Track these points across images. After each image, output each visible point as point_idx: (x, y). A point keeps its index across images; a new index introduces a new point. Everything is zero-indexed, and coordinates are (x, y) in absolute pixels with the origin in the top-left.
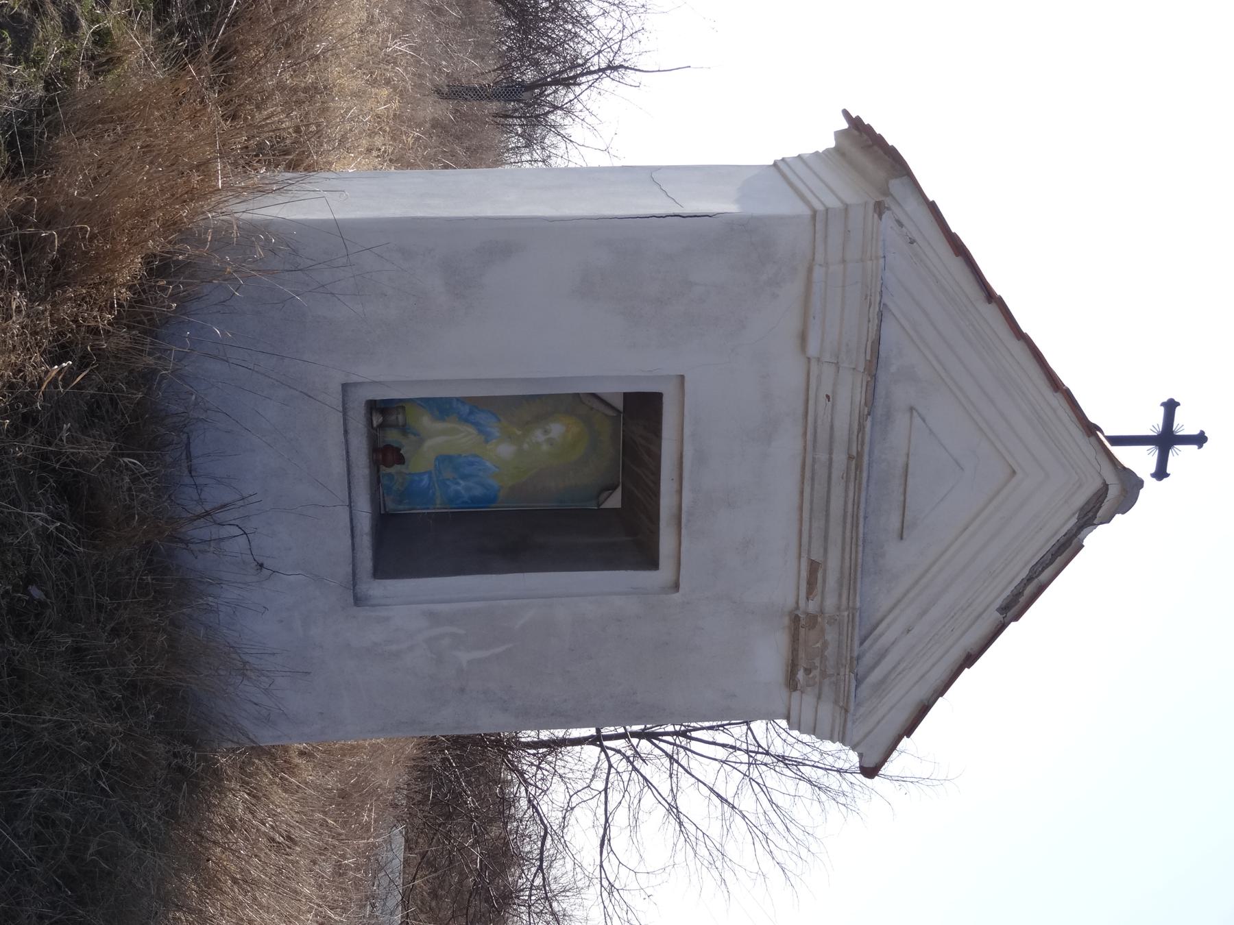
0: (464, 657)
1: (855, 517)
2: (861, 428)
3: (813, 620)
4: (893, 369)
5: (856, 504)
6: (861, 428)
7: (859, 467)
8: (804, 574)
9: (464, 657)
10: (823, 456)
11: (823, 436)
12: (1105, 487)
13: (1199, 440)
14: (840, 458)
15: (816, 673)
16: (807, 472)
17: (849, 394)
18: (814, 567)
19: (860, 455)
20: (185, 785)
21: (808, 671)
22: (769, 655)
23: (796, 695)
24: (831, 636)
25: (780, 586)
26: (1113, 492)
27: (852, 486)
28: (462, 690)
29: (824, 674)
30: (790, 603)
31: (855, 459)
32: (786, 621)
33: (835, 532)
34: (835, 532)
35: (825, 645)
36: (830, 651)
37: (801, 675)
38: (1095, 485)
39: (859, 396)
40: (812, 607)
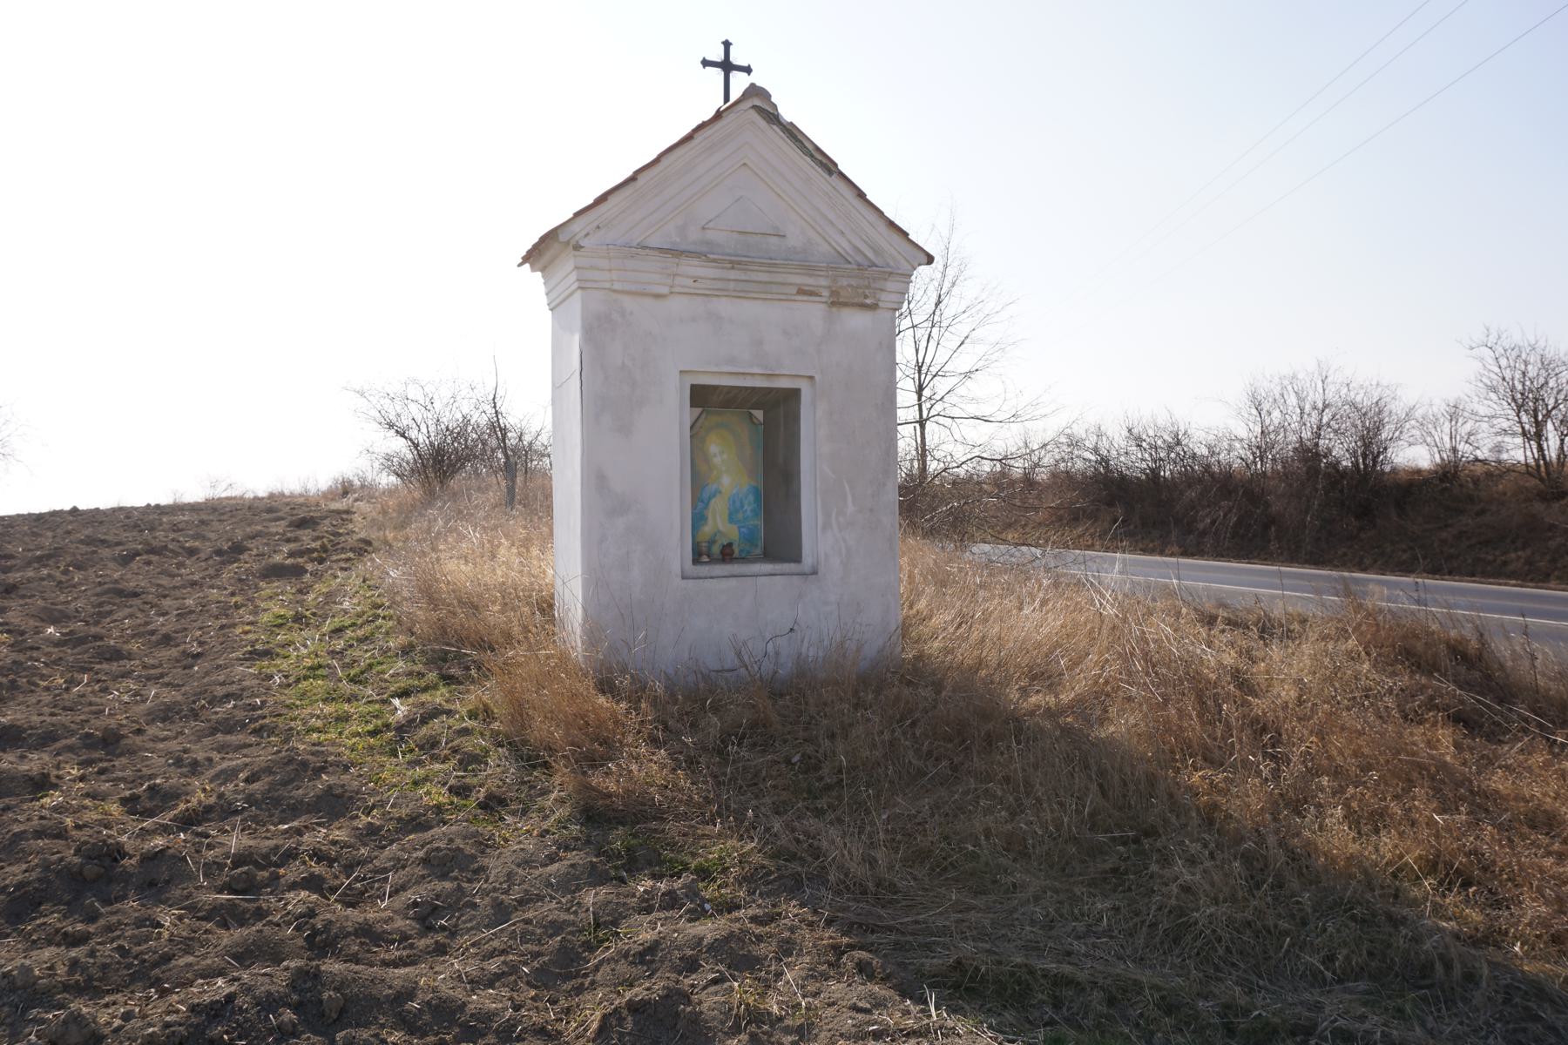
1: (770, 265)
2: (714, 261)
3: (834, 293)
5: (762, 264)
6: (714, 261)
7: (739, 263)
10: (732, 285)
11: (719, 285)
12: (754, 107)
14: (733, 274)
16: (740, 295)
17: (692, 268)
18: (801, 292)
19: (731, 262)
21: (866, 297)
22: (855, 320)
24: (844, 282)
25: (813, 313)
26: (757, 102)
28: (871, 510)
29: (868, 287)
31: (734, 265)
33: (779, 278)
34: (779, 278)
36: (854, 282)
37: (868, 301)
38: (753, 113)
39: (695, 262)
40: (826, 293)
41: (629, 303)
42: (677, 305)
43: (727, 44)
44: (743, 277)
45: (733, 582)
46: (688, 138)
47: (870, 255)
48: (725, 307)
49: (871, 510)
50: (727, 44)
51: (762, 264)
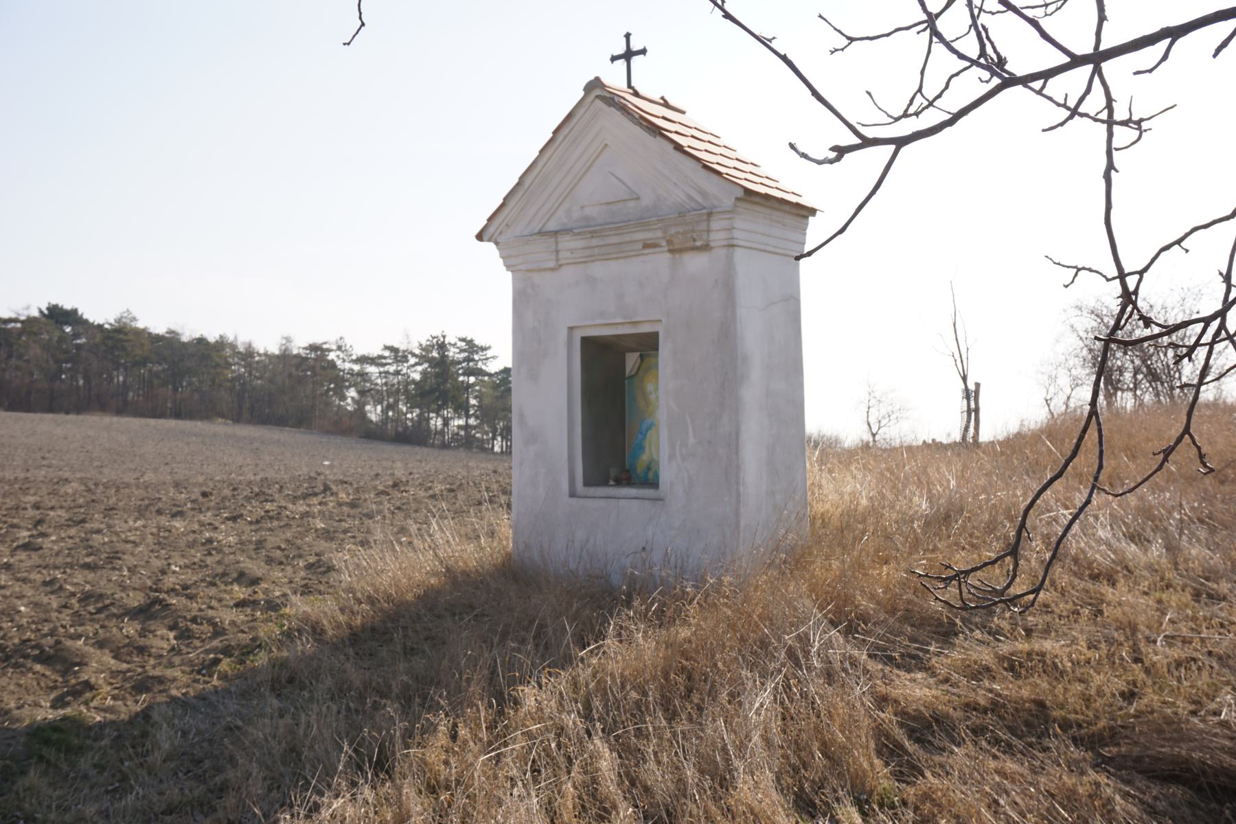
0: (692, 441)
1: (616, 229)
2: (579, 234)
3: (669, 242)
4: (566, 220)
5: (611, 229)
6: (579, 234)
7: (595, 232)
8: (651, 250)
9: (692, 441)
10: (596, 251)
11: (588, 252)
12: (597, 97)
13: (643, 52)
14: (594, 242)
15: (694, 235)
16: (605, 258)
17: (567, 243)
18: (646, 246)
19: (590, 232)
20: (953, 483)
21: (694, 240)
22: (696, 263)
23: (712, 244)
24: (673, 231)
25: (661, 259)
26: (598, 92)
27: (619, 230)
28: (709, 442)
29: (693, 231)
30: (668, 255)
31: (593, 234)
32: (677, 256)
33: (627, 238)
34: (627, 238)
35: (678, 233)
36: (680, 229)
37: (698, 244)
38: (599, 103)
39: (568, 237)
40: (664, 244)
41: (536, 278)
42: (568, 273)
43: (614, 59)
44: (602, 243)
45: (602, 503)
46: (551, 141)
47: (699, 199)
48: (598, 269)
49: (709, 442)
50: (614, 59)
51: (611, 229)
